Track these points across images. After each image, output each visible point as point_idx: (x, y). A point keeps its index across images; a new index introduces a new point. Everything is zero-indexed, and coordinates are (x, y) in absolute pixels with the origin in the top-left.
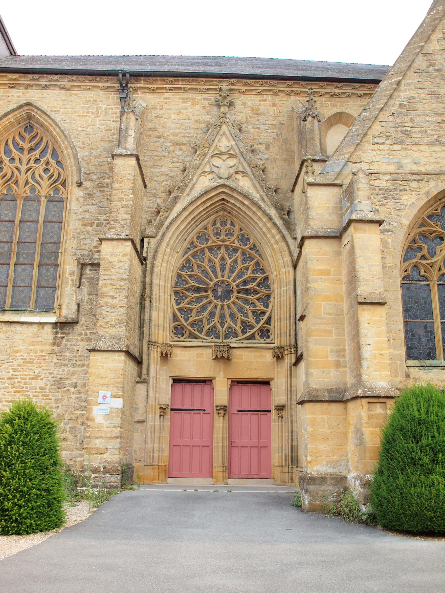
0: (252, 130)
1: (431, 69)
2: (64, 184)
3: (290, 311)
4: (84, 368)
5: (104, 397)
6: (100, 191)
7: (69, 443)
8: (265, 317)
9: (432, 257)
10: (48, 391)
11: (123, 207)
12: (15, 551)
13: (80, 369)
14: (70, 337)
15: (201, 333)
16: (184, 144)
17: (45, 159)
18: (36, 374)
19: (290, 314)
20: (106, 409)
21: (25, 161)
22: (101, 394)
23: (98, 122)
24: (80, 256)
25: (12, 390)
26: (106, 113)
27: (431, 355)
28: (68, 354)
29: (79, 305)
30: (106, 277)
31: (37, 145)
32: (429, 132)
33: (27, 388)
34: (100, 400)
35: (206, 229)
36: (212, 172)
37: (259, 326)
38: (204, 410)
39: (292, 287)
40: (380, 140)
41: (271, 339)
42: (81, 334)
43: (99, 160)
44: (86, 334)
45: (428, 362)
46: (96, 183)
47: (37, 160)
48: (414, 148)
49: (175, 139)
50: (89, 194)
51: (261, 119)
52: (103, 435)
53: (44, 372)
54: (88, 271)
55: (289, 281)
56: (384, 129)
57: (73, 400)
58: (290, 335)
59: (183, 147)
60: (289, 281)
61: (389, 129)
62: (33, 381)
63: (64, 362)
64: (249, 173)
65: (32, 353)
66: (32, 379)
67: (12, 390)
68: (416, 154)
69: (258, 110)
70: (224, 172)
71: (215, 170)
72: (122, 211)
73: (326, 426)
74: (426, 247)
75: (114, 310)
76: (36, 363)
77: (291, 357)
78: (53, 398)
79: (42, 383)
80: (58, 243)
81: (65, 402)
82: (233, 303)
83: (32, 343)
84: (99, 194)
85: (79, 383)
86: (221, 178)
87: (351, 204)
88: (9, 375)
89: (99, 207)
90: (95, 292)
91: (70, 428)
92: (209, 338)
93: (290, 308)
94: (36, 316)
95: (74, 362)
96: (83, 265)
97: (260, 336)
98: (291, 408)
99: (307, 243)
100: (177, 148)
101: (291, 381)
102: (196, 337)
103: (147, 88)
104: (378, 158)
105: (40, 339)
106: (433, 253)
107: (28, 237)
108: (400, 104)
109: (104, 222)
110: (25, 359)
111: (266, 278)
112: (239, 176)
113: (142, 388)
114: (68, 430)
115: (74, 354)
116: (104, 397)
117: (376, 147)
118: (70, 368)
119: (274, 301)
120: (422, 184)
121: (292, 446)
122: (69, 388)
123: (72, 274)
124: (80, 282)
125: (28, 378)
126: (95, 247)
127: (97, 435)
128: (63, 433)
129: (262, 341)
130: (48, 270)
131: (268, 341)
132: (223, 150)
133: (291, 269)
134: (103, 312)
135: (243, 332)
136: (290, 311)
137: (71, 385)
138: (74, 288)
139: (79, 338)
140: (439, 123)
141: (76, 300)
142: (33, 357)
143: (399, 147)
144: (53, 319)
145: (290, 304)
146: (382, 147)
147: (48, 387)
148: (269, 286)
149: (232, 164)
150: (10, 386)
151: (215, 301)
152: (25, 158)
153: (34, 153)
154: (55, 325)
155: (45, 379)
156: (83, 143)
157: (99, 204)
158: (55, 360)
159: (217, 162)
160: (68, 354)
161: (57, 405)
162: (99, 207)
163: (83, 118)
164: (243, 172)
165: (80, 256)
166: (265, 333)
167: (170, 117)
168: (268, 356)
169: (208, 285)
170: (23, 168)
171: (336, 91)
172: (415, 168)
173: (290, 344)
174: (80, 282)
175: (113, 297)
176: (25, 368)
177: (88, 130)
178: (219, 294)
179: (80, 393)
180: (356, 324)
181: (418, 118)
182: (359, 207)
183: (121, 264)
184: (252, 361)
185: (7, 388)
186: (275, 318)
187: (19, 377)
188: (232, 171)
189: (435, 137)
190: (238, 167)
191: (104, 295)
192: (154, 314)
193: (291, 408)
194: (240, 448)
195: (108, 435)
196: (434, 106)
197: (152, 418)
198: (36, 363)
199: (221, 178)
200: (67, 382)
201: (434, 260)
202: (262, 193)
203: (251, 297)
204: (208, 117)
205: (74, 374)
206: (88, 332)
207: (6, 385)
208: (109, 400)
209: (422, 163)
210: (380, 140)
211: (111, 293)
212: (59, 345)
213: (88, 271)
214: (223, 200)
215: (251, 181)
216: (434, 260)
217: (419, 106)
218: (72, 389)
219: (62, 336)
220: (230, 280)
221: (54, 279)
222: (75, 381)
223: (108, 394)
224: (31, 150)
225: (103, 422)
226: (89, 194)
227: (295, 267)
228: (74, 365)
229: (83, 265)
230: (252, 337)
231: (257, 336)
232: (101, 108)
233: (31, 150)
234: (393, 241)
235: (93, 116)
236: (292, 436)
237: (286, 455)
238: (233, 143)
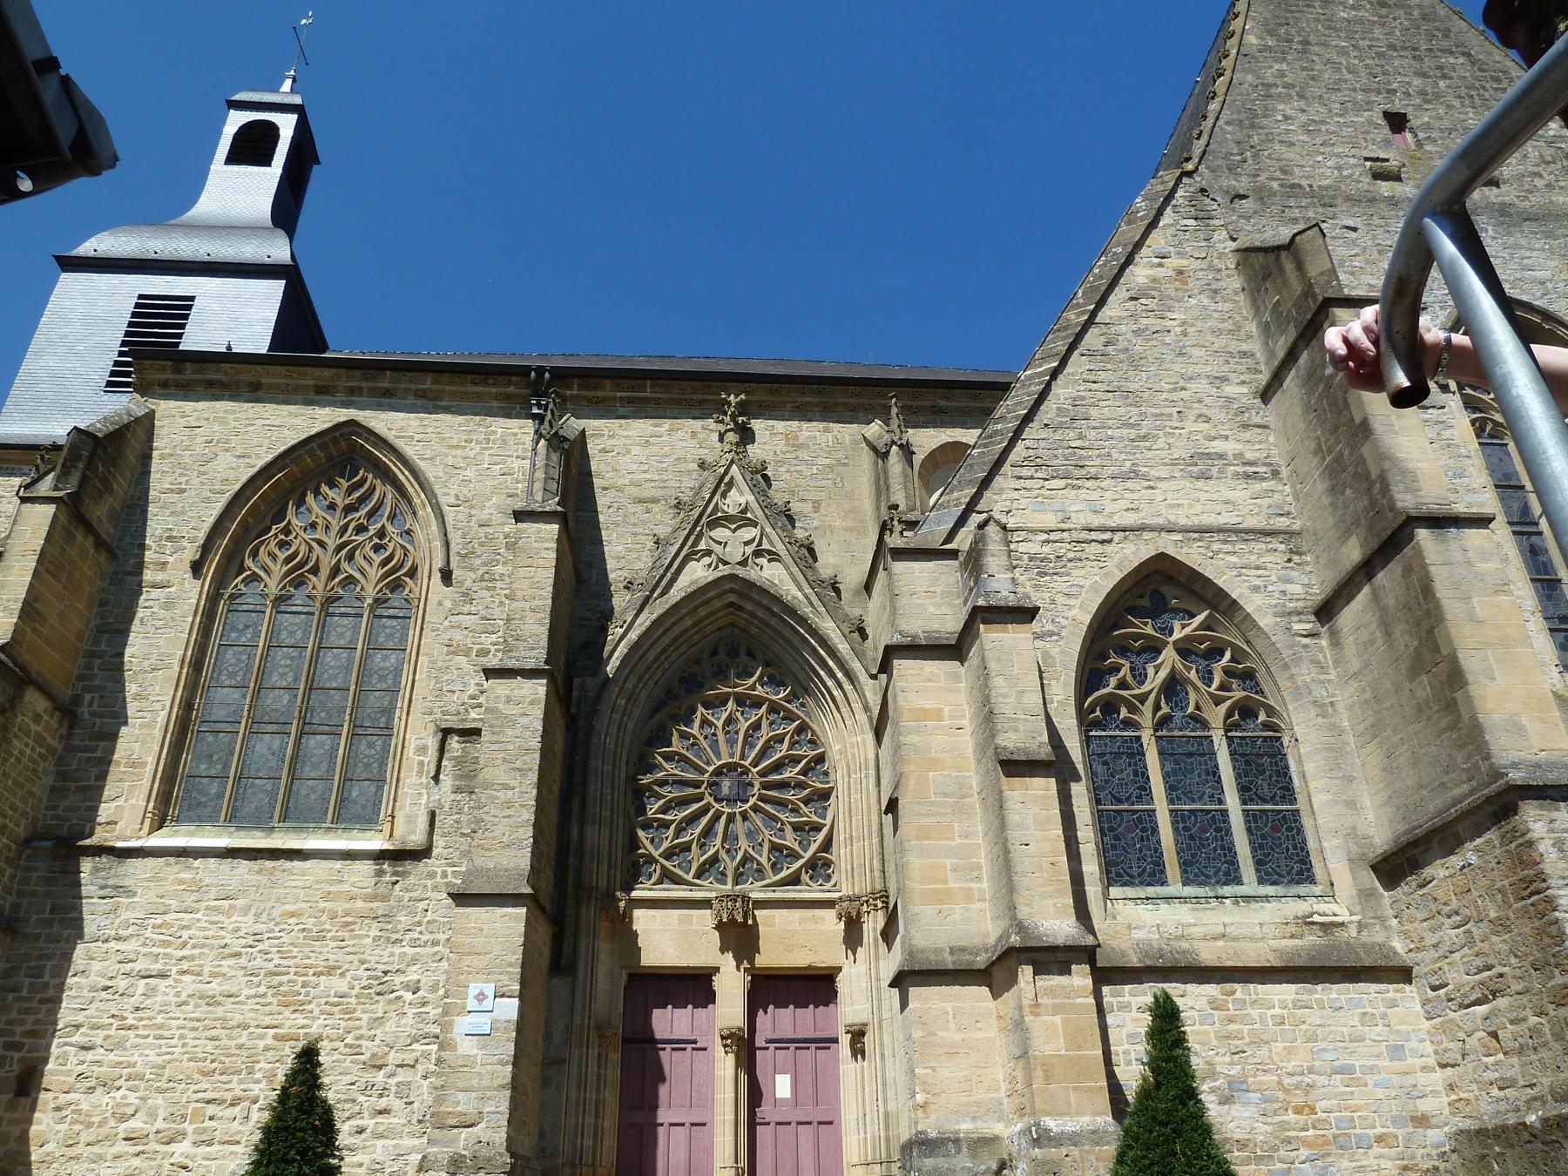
0: (787, 476)
1: (1110, 349)
2: (412, 573)
3: (869, 820)
4: (436, 949)
5: (481, 997)
6: (488, 589)
7: (393, 1120)
8: (821, 836)
9: (1142, 683)
10: (353, 1000)
11: (532, 610)
12: (367, 413)
13: (429, 950)
14: (412, 880)
15: (687, 872)
16: (655, 501)
17: (379, 526)
18: (331, 963)
19: (870, 827)
20: (482, 1023)
21: (335, 528)
22: (474, 989)
23: (487, 459)
24: (439, 715)
25: (275, 1001)
26: (505, 442)
27: (1156, 876)
28: (403, 919)
29: (432, 816)
30: (496, 747)
31: (362, 500)
32: (1115, 456)
33: (307, 994)
34: (472, 1004)
35: (697, 663)
36: (708, 553)
37: (807, 855)
38: (695, 1042)
39: (872, 772)
40: (1025, 472)
41: (832, 882)
42: (432, 875)
43: (487, 529)
44: (444, 875)
45: (1151, 891)
46: (480, 572)
47: (361, 529)
48: (1088, 484)
49: (635, 492)
50: (465, 595)
51: (804, 455)
52: (475, 1082)
53: (350, 958)
54: (454, 743)
55: (866, 760)
56: (1031, 452)
57: (408, 1020)
58: (872, 871)
59: (656, 508)
60: (866, 760)
61: (1040, 452)
62: (323, 978)
63: (394, 936)
64: (780, 548)
65: (324, 918)
66: (321, 974)
67: (275, 1001)
68: (1095, 495)
69: (796, 438)
70: (735, 552)
71: (717, 548)
72: (531, 618)
73: (953, 1026)
74: (1128, 665)
75: (508, 812)
76: (333, 939)
77: (875, 917)
78: (365, 1017)
79: (340, 985)
80: (394, 691)
81: (390, 1026)
82: (755, 809)
83: (327, 896)
84: (485, 593)
85: (424, 980)
86: (726, 563)
87: (976, 583)
88: (271, 966)
89: (483, 618)
90: (468, 783)
91: (398, 1084)
92: (706, 883)
93: (869, 813)
94: (341, 837)
95: (417, 935)
96: (446, 733)
97: (811, 878)
98: (880, 1027)
99: (899, 665)
100: (640, 508)
101: (877, 968)
102: (678, 880)
103: (585, 398)
104: (1024, 503)
105: (345, 887)
106: (1141, 678)
107: (331, 678)
108: (1058, 409)
109: (493, 648)
110: (310, 931)
111: (820, 759)
112: (763, 561)
113: (561, 984)
114: (394, 1089)
115: (417, 919)
116: (481, 997)
117: (1021, 484)
118: (407, 949)
119: (838, 805)
120: (1109, 548)
121: (887, 1115)
122: (401, 993)
123: (422, 750)
124: (439, 767)
125: (311, 972)
126: (473, 697)
127: (461, 1085)
128: (381, 1096)
129: (815, 886)
130: (371, 745)
131: (828, 886)
132: (732, 511)
133: (870, 737)
134: (485, 817)
135: (776, 868)
136: (869, 820)
137: (406, 987)
138: (424, 780)
139: (429, 883)
140: (1133, 441)
141: (428, 801)
142: (327, 926)
143: (1062, 483)
144: (376, 843)
145: (869, 807)
146: (1028, 484)
147: (354, 992)
148: (826, 774)
149: (748, 537)
150: (270, 992)
151: (717, 806)
152: (336, 522)
153: (357, 515)
154: (381, 856)
155: (348, 975)
156: (457, 496)
157: (483, 613)
158: (374, 932)
159: (721, 533)
160: (403, 919)
161: (373, 1032)
162: (483, 618)
163: (459, 452)
164: (770, 552)
165: (439, 715)
166: (819, 867)
167: (628, 451)
168: (830, 924)
169: (702, 771)
170: (332, 543)
171: (942, 403)
172: (1097, 521)
173: (873, 887)
174: (439, 767)
175: (507, 787)
176: (306, 950)
177: (468, 473)
178: (725, 790)
179: (424, 1004)
180: (1001, 805)
181: (1093, 433)
182: (993, 585)
183: (525, 720)
184: (794, 938)
185: (264, 995)
186: (840, 837)
187: (293, 970)
188: (749, 550)
189: (1128, 464)
190: (760, 544)
191: (487, 785)
192: (591, 833)
193: (880, 1027)
194: (772, 1125)
195: (485, 1083)
196: (1122, 410)
197: (580, 1056)
198: (333, 939)
199: (726, 563)
200: (398, 979)
201: (1146, 688)
202: (808, 591)
203: (789, 795)
204: (701, 451)
205: (414, 960)
206: (450, 870)
207: (262, 989)
208: (488, 1004)
209: (1106, 512)
210: (1025, 472)
211: (504, 779)
212: (385, 899)
213: (454, 743)
214: (731, 605)
215: (787, 568)
216: (1146, 688)
217: (1094, 412)
218: (408, 996)
219: (394, 879)
220: (746, 763)
221: (383, 765)
222: (415, 977)
223: (490, 990)
224: (349, 509)
225: (475, 1051)
226: (465, 595)
227: (878, 734)
228: (414, 943)
229: (446, 733)
230: (794, 880)
231: (805, 877)
232: (494, 432)
233: (349, 509)
234: (1062, 652)
235: (478, 448)
236: (884, 1090)
237: (873, 1137)
238: (751, 498)
